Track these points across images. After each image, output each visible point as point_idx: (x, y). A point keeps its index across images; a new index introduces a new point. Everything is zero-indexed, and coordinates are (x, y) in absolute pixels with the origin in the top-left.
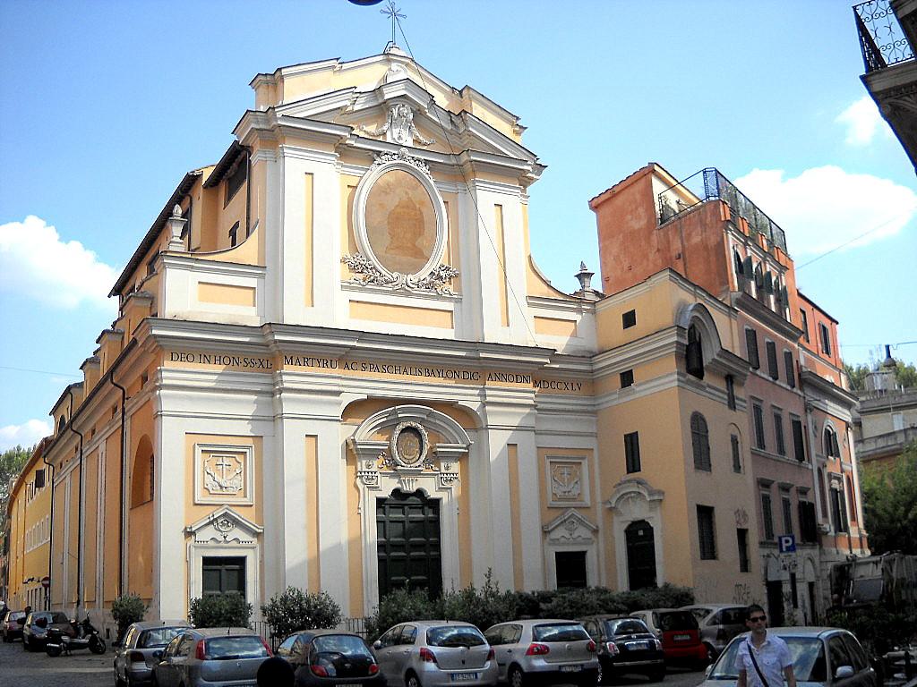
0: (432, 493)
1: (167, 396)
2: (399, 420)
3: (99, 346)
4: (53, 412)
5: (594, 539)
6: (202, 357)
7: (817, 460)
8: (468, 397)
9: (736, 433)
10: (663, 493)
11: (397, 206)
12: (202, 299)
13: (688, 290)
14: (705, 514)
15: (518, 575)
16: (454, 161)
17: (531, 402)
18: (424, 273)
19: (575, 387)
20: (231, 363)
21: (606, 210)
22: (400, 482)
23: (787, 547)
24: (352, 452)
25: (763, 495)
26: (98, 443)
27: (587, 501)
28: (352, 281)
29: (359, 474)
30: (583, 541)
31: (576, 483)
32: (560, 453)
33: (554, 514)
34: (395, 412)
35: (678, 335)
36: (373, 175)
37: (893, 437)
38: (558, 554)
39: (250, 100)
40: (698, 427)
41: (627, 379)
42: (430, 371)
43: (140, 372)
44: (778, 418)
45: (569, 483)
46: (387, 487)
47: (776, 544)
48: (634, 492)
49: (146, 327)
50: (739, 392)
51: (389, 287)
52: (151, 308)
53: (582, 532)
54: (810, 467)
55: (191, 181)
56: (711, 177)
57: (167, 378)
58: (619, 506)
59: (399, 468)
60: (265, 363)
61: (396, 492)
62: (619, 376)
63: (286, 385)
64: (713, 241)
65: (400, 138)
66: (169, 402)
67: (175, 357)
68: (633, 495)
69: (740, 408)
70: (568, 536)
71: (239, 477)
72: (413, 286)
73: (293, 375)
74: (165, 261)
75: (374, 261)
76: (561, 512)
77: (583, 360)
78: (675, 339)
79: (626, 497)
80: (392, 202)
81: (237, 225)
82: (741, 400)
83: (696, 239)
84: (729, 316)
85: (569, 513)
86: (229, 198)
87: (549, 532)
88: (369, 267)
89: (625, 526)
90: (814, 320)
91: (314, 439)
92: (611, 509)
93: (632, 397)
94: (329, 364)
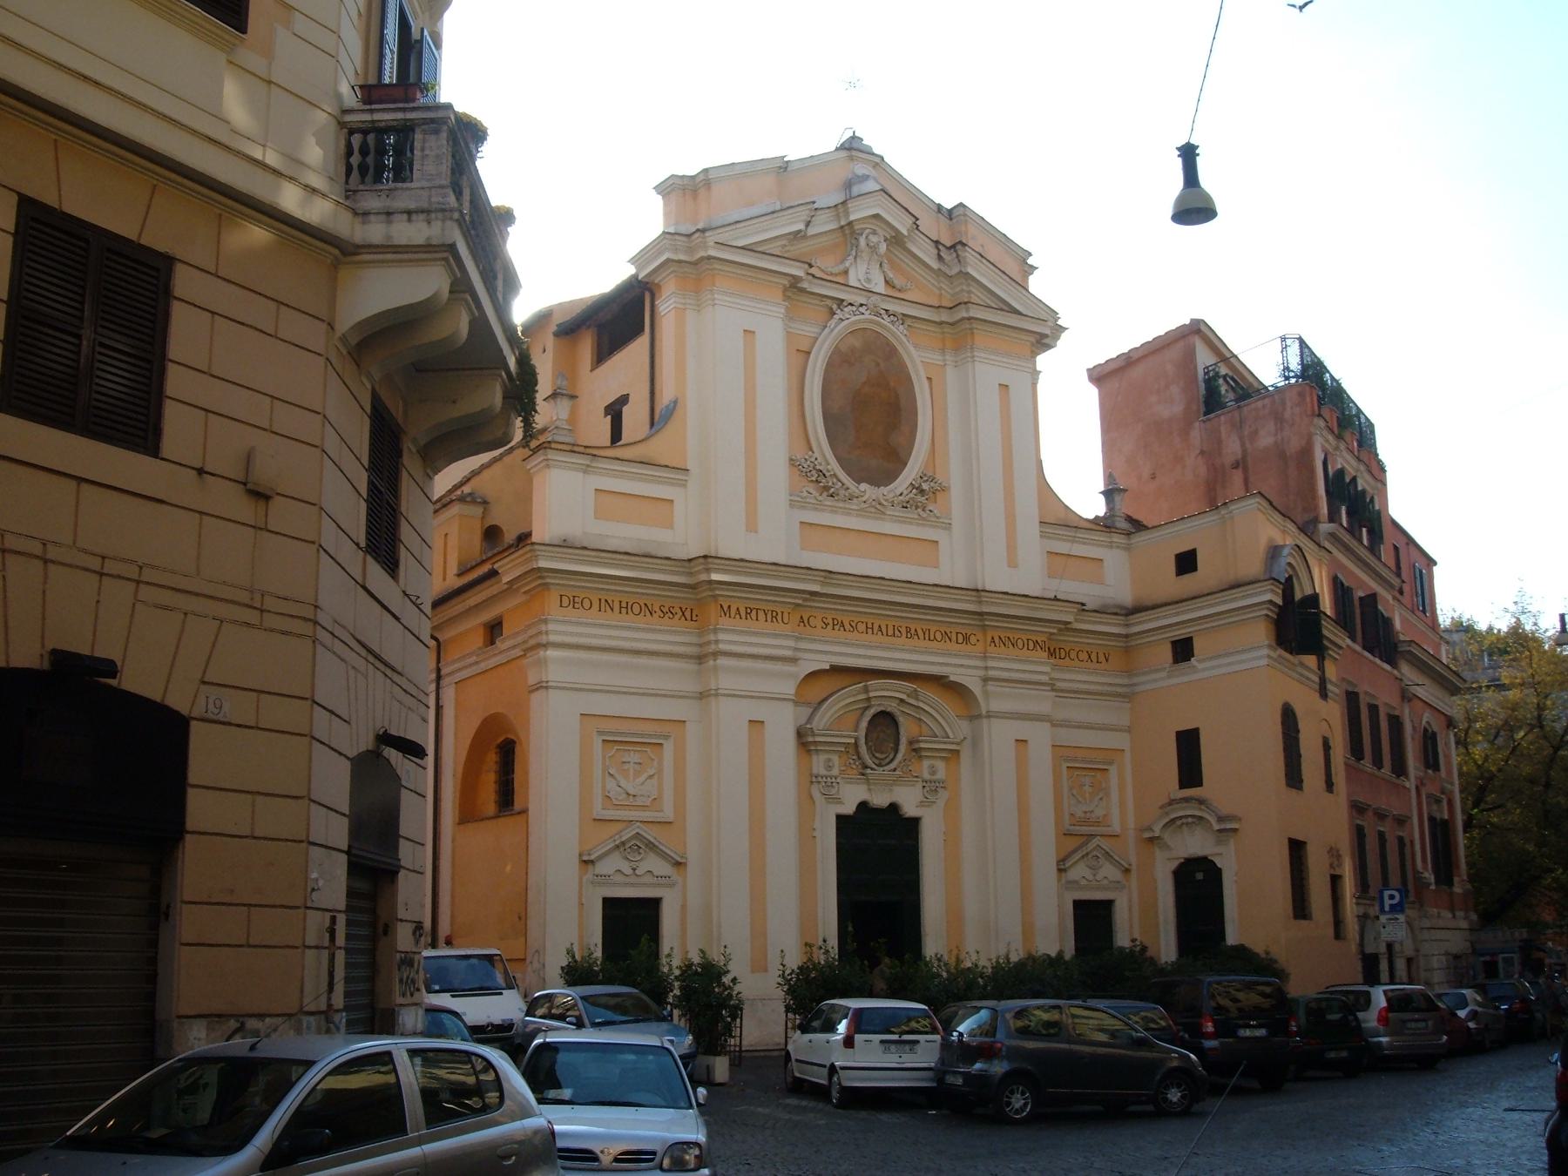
0: (910, 810)
6: (603, 601)
8: (961, 667)
10: (1240, 819)
11: (865, 383)
12: (599, 514)
15: (1028, 930)
17: (1044, 678)
23: (1391, 906)
25: (1358, 825)
27: (1116, 827)
29: (814, 779)
31: (1101, 799)
38: (608, 902)
41: (1183, 650)
42: (913, 631)
43: (487, 616)
45: (637, 774)
46: (851, 797)
47: (1373, 899)
49: (529, 555)
52: (483, 518)
56: (1294, 350)
58: (1166, 836)
60: (688, 614)
61: (863, 806)
62: (1169, 646)
63: (722, 647)
64: (1294, 444)
65: (869, 280)
66: (556, 666)
68: (1190, 820)
72: (885, 503)
75: (835, 466)
77: (1114, 619)
79: (1179, 823)
81: (624, 400)
83: (1266, 440)
85: (1095, 841)
86: (601, 357)
89: (1175, 864)
91: (206, 680)
92: (1151, 840)
94: (779, 618)
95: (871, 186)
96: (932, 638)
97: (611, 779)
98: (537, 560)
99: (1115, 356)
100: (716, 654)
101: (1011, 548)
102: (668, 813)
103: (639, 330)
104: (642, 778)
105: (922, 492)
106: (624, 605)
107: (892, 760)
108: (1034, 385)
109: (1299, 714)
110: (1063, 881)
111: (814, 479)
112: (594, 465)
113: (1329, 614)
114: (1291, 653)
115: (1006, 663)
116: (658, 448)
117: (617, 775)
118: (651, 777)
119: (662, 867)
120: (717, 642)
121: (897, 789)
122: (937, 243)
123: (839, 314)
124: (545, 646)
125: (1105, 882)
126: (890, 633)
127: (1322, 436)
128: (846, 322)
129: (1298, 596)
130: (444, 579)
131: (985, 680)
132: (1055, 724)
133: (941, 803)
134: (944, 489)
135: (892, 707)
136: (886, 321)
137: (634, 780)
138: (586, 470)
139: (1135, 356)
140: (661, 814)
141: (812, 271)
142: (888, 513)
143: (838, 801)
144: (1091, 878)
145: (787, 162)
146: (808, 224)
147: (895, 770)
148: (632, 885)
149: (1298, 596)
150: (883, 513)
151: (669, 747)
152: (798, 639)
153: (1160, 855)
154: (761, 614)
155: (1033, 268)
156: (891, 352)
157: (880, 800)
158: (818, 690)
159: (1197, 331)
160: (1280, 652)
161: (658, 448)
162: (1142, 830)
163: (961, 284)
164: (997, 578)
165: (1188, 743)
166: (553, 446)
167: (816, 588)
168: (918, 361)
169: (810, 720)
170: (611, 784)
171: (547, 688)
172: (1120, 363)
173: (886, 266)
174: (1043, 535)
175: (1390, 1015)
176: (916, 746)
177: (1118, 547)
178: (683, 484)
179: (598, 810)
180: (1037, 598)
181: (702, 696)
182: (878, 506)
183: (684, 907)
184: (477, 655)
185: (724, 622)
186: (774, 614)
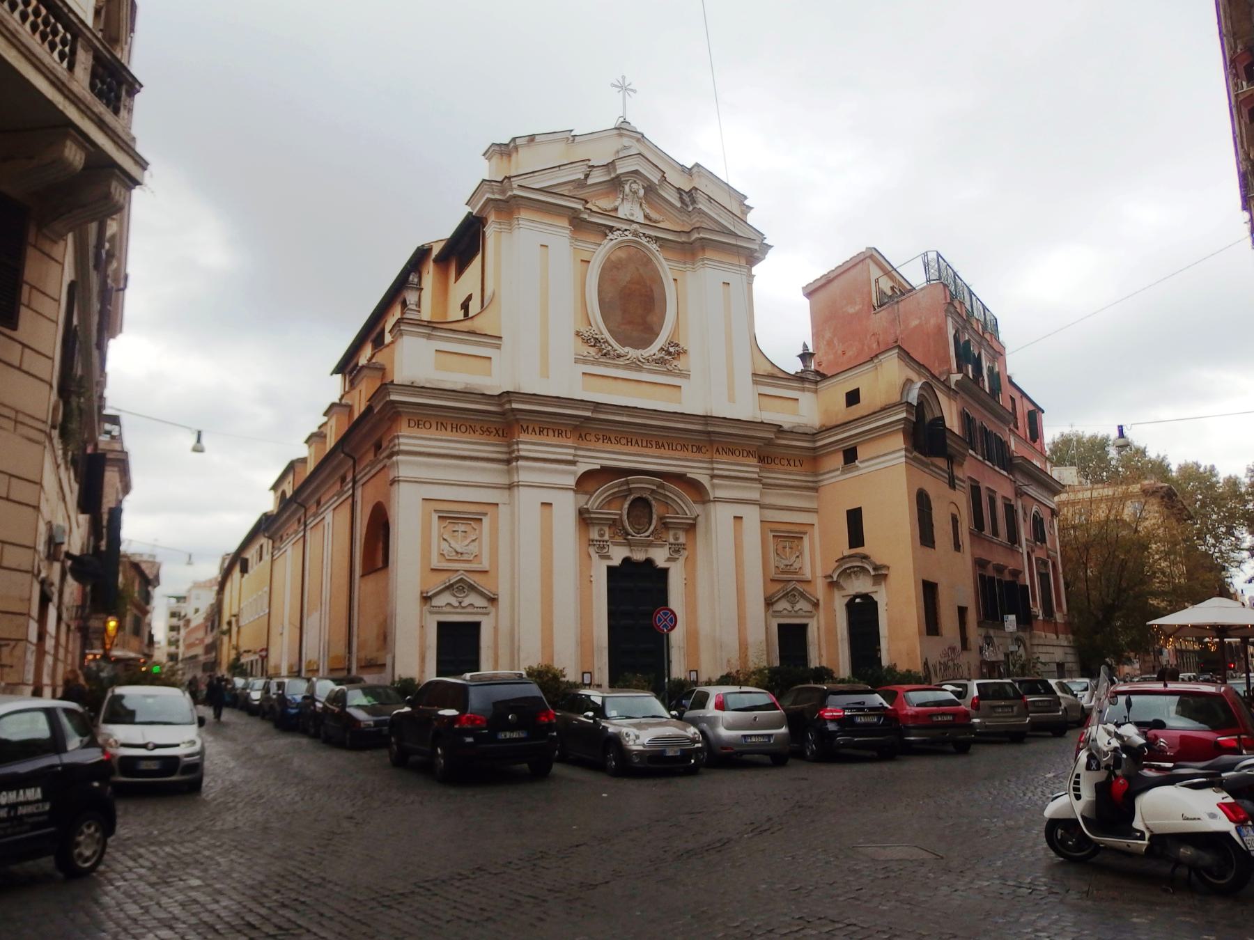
0: (661, 562)
1: (404, 462)
2: (630, 491)
3: (325, 419)
4: (275, 487)
5: (814, 611)
7: (1027, 545)
9: (955, 512)
10: (888, 568)
13: (913, 369)
14: (930, 590)
16: (684, 239)
17: (755, 476)
18: (654, 349)
19: (797, 463)
21: (822, 295)
22: (631, 551)
24: (585, 519)
26: (325, 514)
27: (808, 576)
28: (585, 354)
31: (798, 557)
32: (783, 527)
33: (778, 586)
34: (627, 483)
35: (907, 411)
36: (601, 252)
38: (780, 626)
39: (484, 170)
40: (923, 503)
41: (850, 456)
44: (992, 501)
46: (618, 555)
48: (857, 567)
50: (958, 472)
51: (621, 362)
54: (1021, 551)
55: (421, 255)
57: (405, 443)
58: (841, 581)
59: (630, 537)
61: (626, 560)
63: (522, 453)
66: (405, 468)
67: (412, 424)
68: (855, 569)
69: (961, 489)
70: (789, 608)
71: (798, 559)
73: (528, 445)
74: (402, 328)
75: (607, 335)
78: (904, 415)
80: (625, 277)
81: (470, 298)
82: (960, 480)
84: (949, 398)
86: (460, 272)
88: (602, 341)
90: (1023, 408)
93: (856, 473)
94: (564, 434)
96: (674, 448)
97: (445, 542)
99: (819, 277)
101: (731, 388)
102: (485, 565)
105: (669, 353)
107: (646, 531)
108: (750, 284)
109: (932, 497)
113: (957, 433)
114: (925, 456)
115: (725, 465)
117: (448, 539)
118: (473, 541)
119: (479, 602)
120: (518, 450)
122: (679, 189)
123: (610, 236)
125: (800, 612)
127: (952, 318)
128: (615, 241)
129: (929, 417)
131: (713, 477)
132: (762, 506)
133: (681, 561)
134: (685, 352)
135: (646, 495)
136: (644, 241)
138: (429, 337)
139: (832, 276)
140: (480, 566)
141: (588, 206)
146: (587, 176)
147: (649, 536)
149: (929, 417)
150: (642, 367)
151: (486, 521)
152: (576, 448)
155: (750, 208)
156: (648, 262)
157: (639, 556)
159: (872, 257)
160: (915, 453)
162: (826, 577)
165: (855, 518)
166: (405, 321)
167: (588, 414)
170: (444, 545)
171: (399, 481)
172: (823, 281)
173: (644, 206)
174: (755, 383)
175: (981, 702)
176: (664, 521)
177: (809, 391)
178: (498, 347)
179: (435, 563)
181: (511, 487)
183: (496, 629)
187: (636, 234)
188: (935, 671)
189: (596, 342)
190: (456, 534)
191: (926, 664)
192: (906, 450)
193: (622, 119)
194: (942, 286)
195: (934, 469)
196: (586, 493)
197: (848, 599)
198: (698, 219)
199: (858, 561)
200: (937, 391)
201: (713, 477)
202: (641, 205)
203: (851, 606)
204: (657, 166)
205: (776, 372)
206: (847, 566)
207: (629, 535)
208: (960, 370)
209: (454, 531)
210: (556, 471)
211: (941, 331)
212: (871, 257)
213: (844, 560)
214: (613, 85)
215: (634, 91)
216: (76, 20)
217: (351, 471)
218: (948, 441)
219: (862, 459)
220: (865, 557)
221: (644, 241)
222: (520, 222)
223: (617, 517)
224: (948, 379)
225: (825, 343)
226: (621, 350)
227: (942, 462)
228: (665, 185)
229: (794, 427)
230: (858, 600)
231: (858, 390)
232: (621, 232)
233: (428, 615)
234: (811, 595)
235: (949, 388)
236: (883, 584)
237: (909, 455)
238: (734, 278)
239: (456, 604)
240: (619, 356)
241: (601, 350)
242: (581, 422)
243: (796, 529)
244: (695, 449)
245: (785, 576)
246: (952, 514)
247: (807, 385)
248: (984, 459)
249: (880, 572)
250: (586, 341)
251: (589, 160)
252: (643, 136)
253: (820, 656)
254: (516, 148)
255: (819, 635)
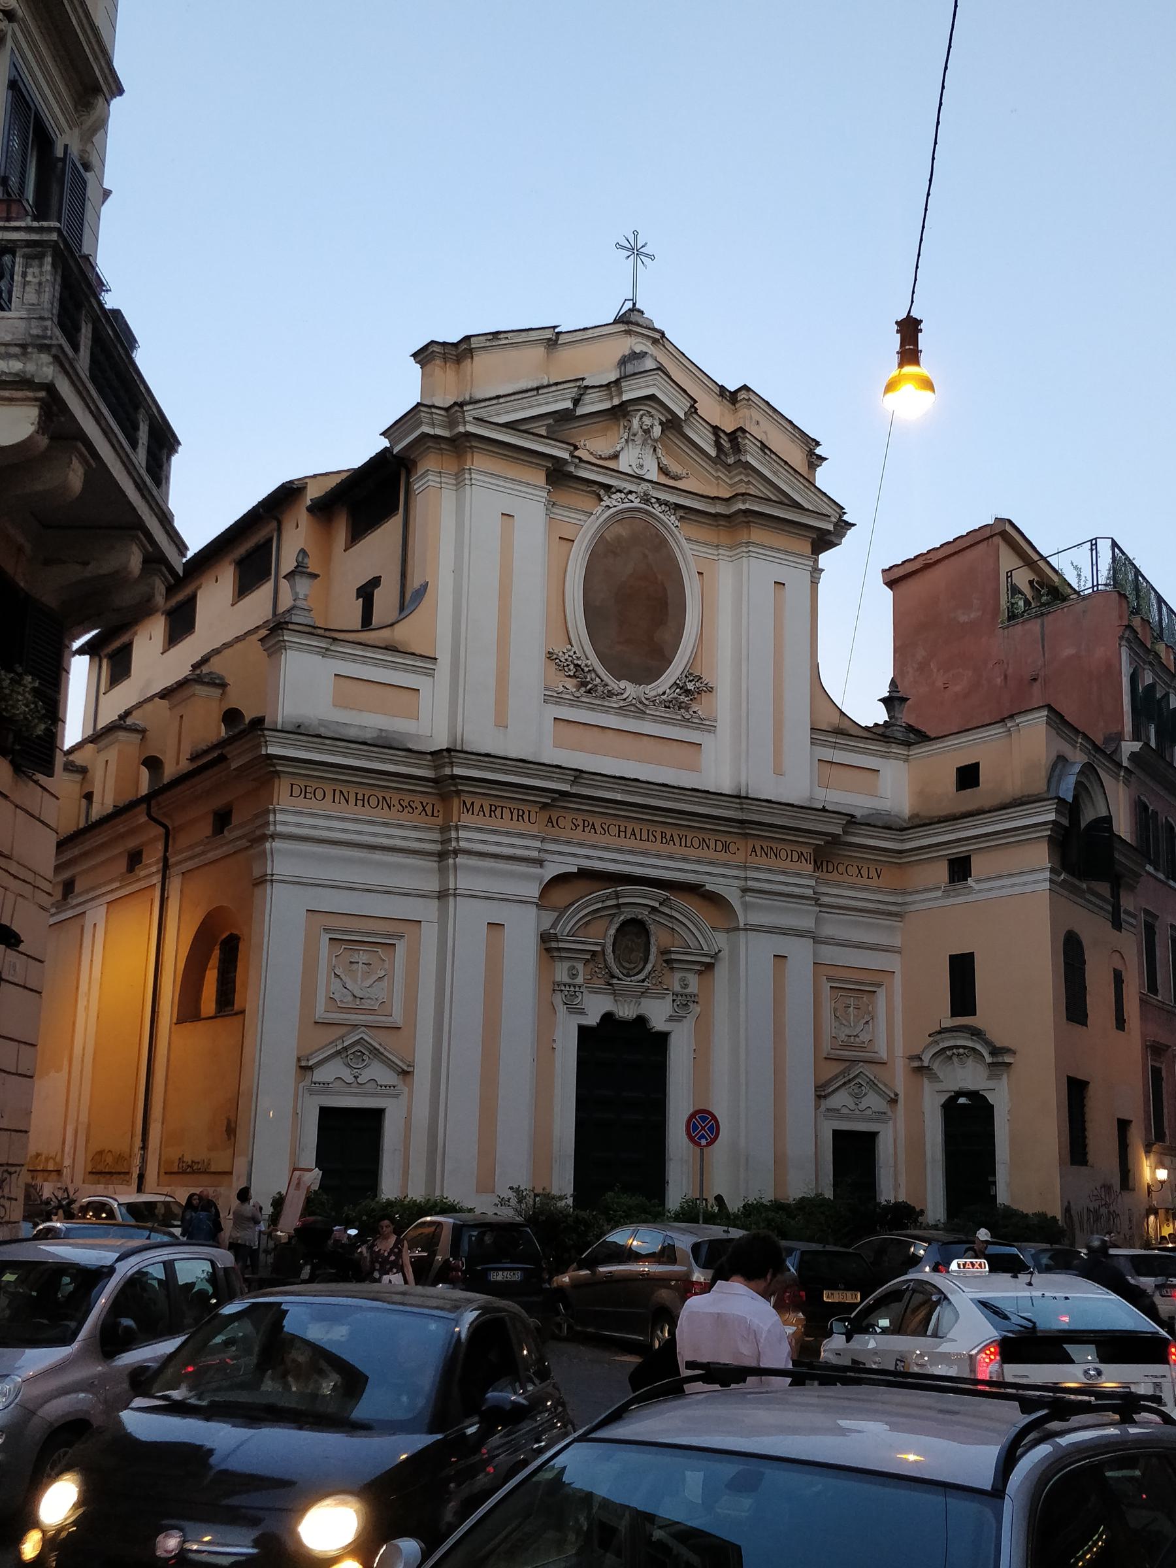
0: (658, 1024)
6: (337, 793)
9: (1120, 967)
10: (1014, 1053)
18: (664, 684)
20: (701, 847)
26: (88, 905)
28: (561, 689)
30: (874, 1116)
31: (867, 1023)
32: (846, 975)
33: (836, 1068)
35: (1057, 811)
37: (100, 1168)
38: (837, 1134)
41: (960, 869)
42: (668, 837)
46: (595, 1008)
48: (964, 1047)
50: (1128, 902)
51: (614, 703)
53: (873, 1101)
60: (429, 809)
61: (608, 1017)
63: (462, 844)
68: (961, 1051)
72: (647, 702)
75: (594, 661)
76: (843, 1066)
78: (1052, 816)
81: (375, 582)
87: (825, 1097)
88: (586, 669)
93: (970, 898)
94: (526, 816)
95: (649, 364)
98: (266, 746)
100: (456, 852)
102: (397, 1017)
103: (391, 510)
104: (370, 981)
105: (687, 692)
106: (360, 797)
108: (814, 583)
109: (1086, 941)
110: (823, 1108)
111: (571, 673)
112: (333, 648)
116: (402, 633)
119: (386, 1076)
120: (458, 839)
121: (645, 1002)
124: (273, 837)
125: (869, 1112)
126: (644, 837)
127: (1131, 648)
130: (178, 763)
131: (745, 890)
132: (816, 940)
134: (710, 690)
135: (643, 914)
136: (657, 510)
137: (362, 982)
138: (325, 653)
139: (935, 557)
142: (648, 712)
143: (582, 1012)
144: (853, 1107)
145: (559, 333)
146: (576, 402)
147: (643, 981)
148: (355, 1094)
149: (1088, 816)
151: (400, 947)
152: (543, 840)
153: (927, 1086)
154: (506, 813)
156: (661, 544)
157: (626, 1011)
158: (560, 896)
161: (402, 633)
162: (911, 1058)
163: (741, 473)
164: (766, 787)
166: (290, 626)
167: (565, 787)
168: (689, 553)
169: (554, 926)
174: (814, 742)
177: (896, 758)
178: (430, 673)
179: (320, 1013)
180: (802, 807)
181: (443, 895)
182: (640, 706)
184: (121, 881)
185: (467, 819)
186: (521, 813)
187: (646, 499)
188: (1081, 1223)
189: (579, 672)
190: (355, 966)
191: (1067, 1210)
192: (1052, 870)
193: (629, 305)
194: (1116, 594)
195: (1093, 899)
196: (553, 909)
197: (947, 1096)
198: (742, 477)
199: (966, 1039)
200: (1099, 770)
201: (745, 890)
202: (655, 450)
203: (950, 1107)
204: (685, 391)
205: (845, 725)
206: (946, 1044)
207: (613, 977)
208: (1136, 737)
209: (351, 962)
210: (512, 875)
211: (1112, 671)
212: (1004, 535)
213: (943, 1035)
214: (619, 246)
215: (652, 257)
216: (143, 390)
217: (160, 846)
218: (1117, 855)
219: (979, 878)
220: (976, 1033)
221: (657, 510)
222: (473, 476)
223: (598, 948)
224: (1117, 749)
225: (916, 666)
226: (614, 684)
227: (1104, 888)
228: (694, 419)
229: (870, 815)
230: (962, 1100)
231: (977, 765)
232: (623, 496)
233: (307, 1095)
234: (885, 1085)
235: (1119, 765)
236: (1005, 1076)
237: (1055, 878)
238: (796, 577)
239: (350, 1079)
240: (611, 694)
241: (583, 684)
242: (554, 800)
243: (863, 977)
244: (719, 847)
245: (847, 1053)
246: (1115, 970)
247: (895, 749)
248: (1168, 878)
249: (1000, 1060)
250: (561, 668)
251: (583, 379)
252: (663, 335)
253: (897, 1186)
254: (470, 352)
255: (895, 1153)
